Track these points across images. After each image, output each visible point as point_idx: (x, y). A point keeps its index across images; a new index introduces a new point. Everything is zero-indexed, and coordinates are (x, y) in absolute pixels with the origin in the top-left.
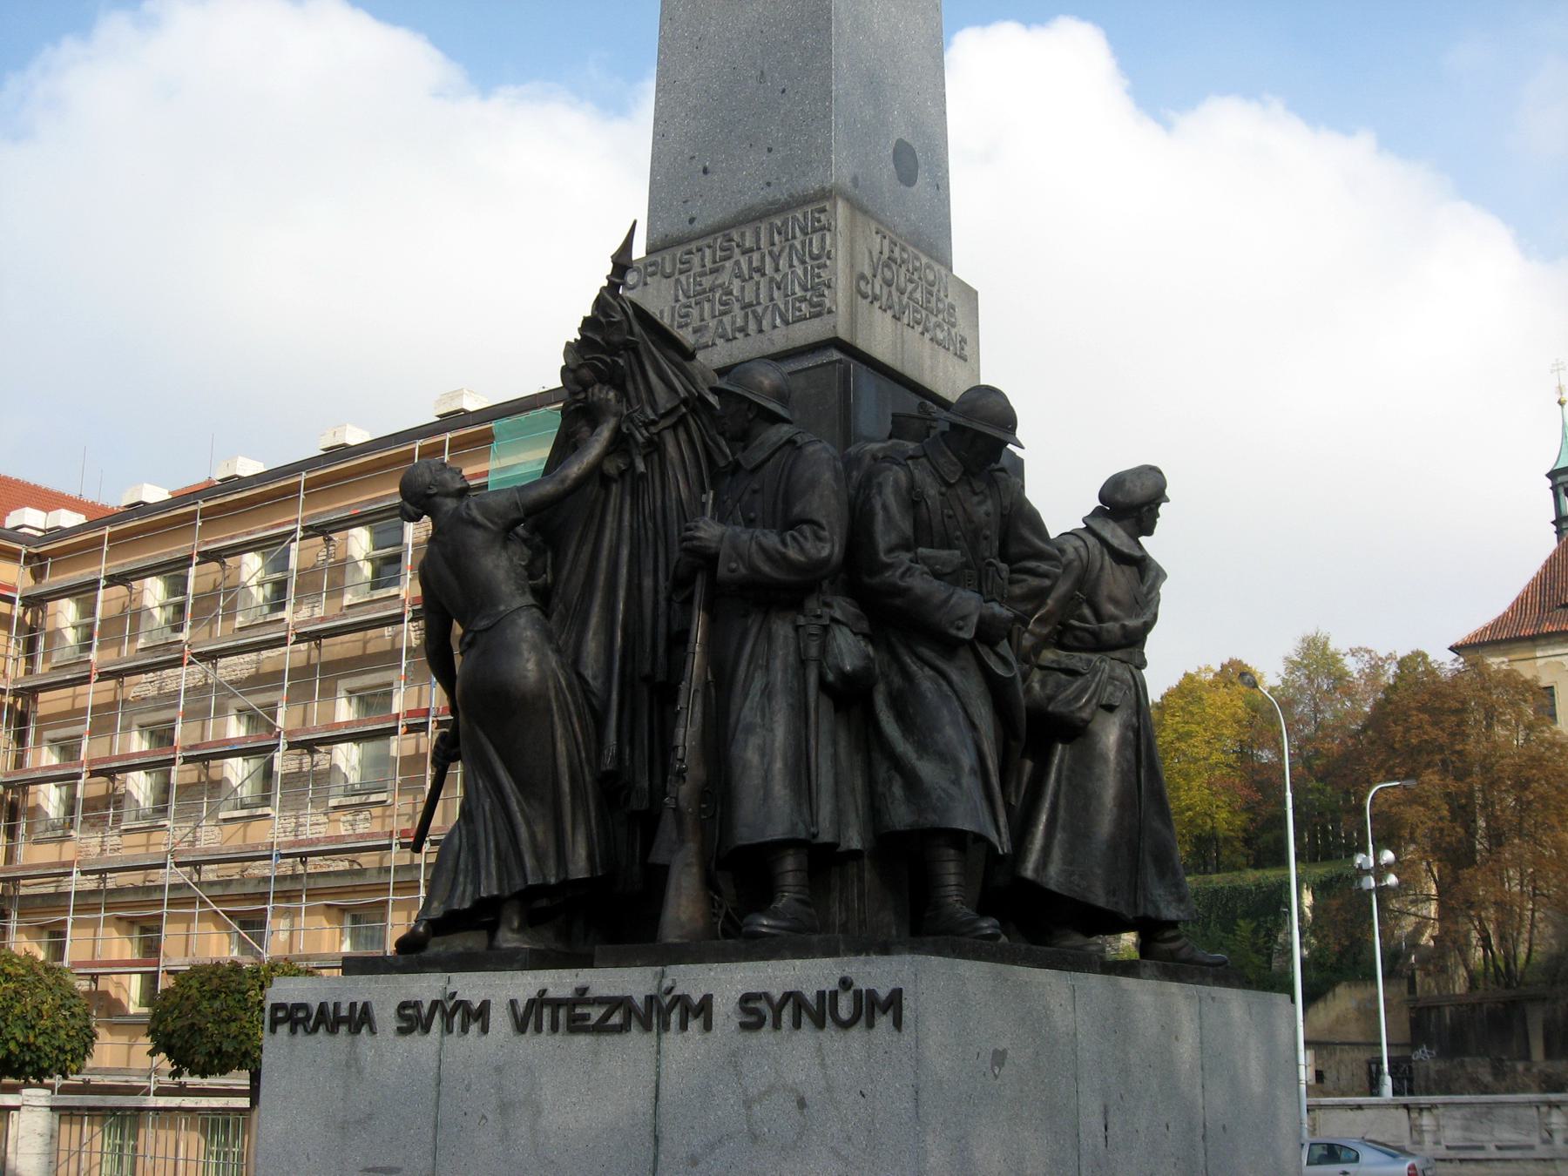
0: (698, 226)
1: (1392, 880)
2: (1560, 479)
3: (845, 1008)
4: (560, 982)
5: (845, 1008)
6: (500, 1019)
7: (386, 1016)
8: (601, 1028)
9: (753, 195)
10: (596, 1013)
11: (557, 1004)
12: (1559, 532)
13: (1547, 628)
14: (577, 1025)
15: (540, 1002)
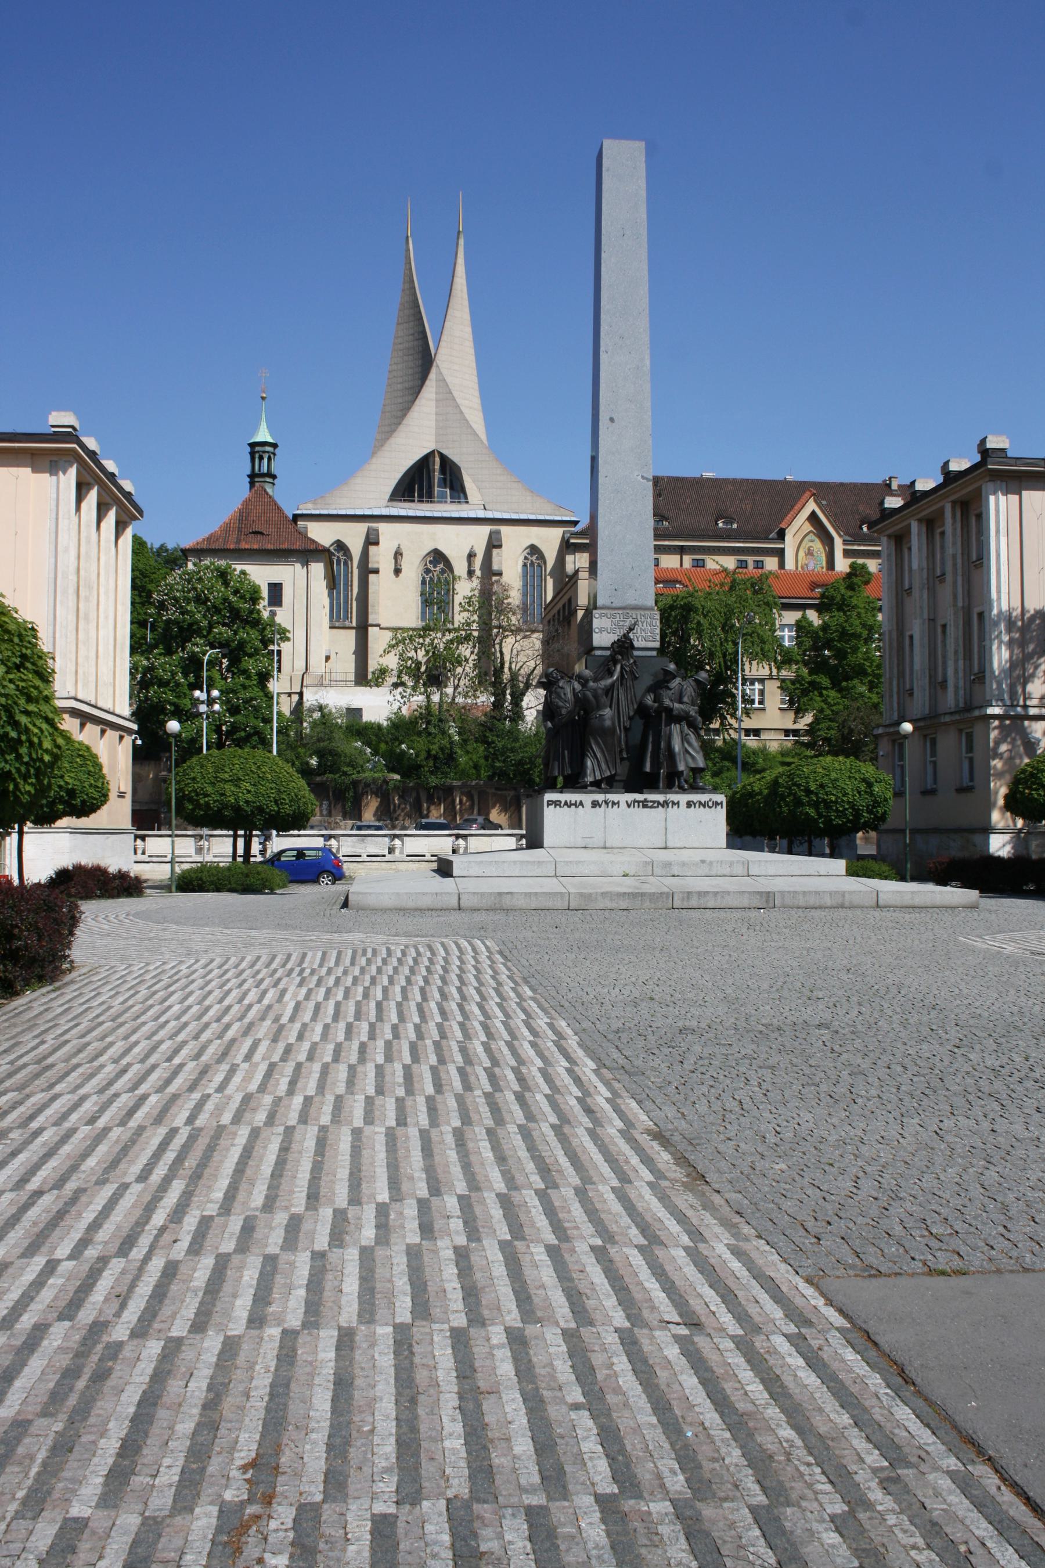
0: (614, 605)
1: (217, 707)
2: (257, 449)
3: (710, 804)
4: (639, 797)
5: (710, 804)
6: (623, 805)
7: (683, 804)
8: (651, 807)
9: (631, 601)
10: (650, 804)
11: (639, 802)
12: (252, 484)
13: (244, 546)
14: (645, 806)
15: (635, 801)
